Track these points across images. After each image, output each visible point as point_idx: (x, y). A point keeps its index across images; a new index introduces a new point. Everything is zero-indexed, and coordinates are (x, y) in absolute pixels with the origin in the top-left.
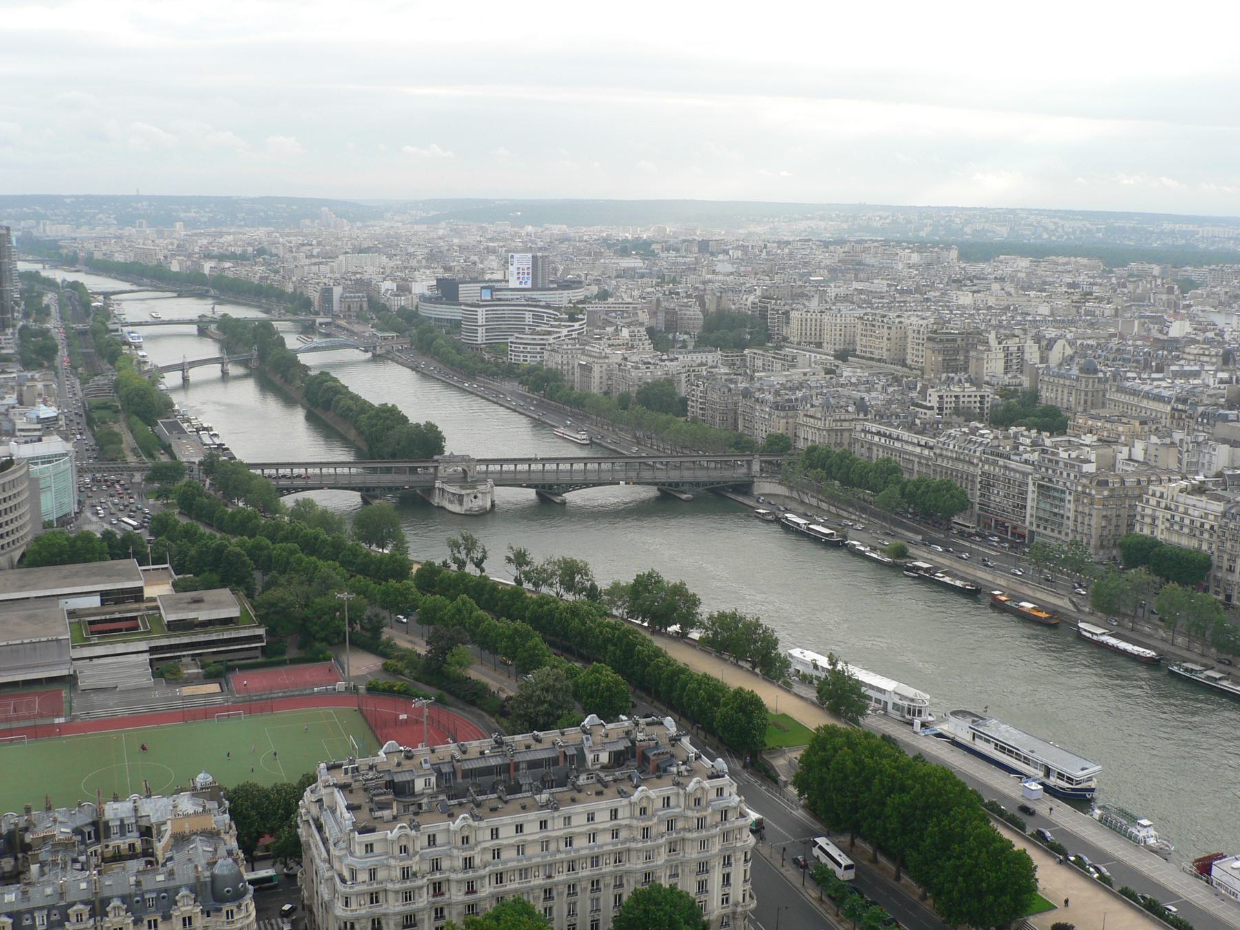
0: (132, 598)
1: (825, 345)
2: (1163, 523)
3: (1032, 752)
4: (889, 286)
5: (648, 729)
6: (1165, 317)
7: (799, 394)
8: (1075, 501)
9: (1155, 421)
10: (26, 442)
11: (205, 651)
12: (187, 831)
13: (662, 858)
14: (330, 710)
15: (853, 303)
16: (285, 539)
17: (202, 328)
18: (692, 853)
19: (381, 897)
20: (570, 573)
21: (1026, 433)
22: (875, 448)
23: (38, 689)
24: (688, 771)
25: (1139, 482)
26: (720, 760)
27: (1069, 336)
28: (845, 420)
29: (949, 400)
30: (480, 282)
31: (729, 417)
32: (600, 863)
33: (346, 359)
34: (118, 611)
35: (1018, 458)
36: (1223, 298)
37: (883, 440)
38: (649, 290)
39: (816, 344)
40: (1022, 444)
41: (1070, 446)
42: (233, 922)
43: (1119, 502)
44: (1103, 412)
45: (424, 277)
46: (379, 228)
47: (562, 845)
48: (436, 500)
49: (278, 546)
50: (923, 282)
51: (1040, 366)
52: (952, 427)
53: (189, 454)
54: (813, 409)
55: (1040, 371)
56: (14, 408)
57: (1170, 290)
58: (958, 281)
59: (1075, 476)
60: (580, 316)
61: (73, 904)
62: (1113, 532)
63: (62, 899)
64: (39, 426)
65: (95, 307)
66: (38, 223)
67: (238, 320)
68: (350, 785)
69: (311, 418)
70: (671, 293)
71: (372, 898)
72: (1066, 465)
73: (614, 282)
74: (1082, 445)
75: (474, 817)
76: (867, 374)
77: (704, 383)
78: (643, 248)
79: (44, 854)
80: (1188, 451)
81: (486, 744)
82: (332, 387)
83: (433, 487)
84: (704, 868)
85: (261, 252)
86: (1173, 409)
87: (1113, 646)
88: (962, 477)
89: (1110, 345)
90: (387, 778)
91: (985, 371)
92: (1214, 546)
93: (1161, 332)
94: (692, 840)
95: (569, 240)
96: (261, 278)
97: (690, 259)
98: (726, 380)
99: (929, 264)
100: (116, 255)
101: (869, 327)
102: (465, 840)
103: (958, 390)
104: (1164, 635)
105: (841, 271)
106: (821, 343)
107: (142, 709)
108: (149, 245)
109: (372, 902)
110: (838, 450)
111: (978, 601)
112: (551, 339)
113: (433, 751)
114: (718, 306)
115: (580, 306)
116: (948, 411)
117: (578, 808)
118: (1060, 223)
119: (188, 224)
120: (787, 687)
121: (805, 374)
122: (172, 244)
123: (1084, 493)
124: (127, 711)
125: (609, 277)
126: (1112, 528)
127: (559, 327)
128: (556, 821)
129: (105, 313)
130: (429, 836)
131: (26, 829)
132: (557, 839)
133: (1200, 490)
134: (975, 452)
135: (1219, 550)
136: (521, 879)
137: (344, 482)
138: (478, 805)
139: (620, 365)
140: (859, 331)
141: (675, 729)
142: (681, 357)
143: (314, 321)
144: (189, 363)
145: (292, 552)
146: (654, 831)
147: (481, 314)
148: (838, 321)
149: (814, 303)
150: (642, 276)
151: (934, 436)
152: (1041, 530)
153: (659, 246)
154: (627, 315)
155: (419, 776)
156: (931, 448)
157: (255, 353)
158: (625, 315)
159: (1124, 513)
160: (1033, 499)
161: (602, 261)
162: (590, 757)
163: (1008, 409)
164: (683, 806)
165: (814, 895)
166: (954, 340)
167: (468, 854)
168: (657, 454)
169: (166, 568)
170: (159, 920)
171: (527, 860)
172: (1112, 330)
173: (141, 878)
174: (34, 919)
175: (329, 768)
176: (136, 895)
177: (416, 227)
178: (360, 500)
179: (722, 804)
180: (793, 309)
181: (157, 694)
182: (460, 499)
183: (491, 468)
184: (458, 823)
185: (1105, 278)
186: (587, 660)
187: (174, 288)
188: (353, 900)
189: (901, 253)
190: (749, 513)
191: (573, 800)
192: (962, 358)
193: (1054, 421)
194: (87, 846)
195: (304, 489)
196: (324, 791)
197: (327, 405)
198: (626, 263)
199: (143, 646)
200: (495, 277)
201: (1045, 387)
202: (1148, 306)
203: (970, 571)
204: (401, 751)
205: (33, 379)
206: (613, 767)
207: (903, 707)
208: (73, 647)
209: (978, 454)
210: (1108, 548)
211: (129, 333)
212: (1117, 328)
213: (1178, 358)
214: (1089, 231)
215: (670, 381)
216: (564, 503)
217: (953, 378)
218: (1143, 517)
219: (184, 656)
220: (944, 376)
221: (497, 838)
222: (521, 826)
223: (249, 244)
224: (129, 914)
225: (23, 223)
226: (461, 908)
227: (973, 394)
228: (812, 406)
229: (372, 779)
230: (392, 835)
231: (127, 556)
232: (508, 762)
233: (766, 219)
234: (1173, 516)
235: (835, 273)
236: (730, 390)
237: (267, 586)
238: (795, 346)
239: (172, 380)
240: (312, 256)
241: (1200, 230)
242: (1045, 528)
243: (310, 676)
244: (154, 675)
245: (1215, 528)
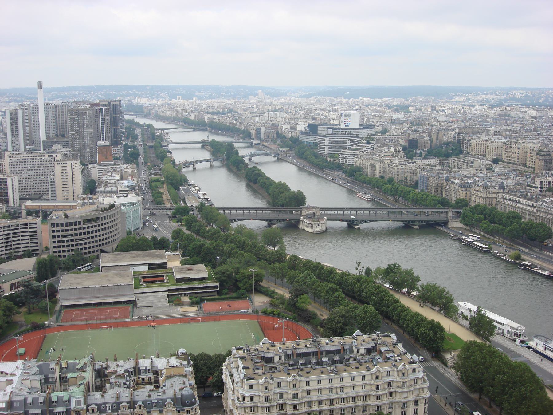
1: (487, 156)
5: (383, 338)
7: (472, 180)
10: (121, 197)
11: (192, 292)
12: (172, 374)
15: (502, 136)
16: (231, 242)
17: (204, 145)
18: (399, 399)
19: (256, 409)
22: (508, 207)
26: (415, 355)
28: (494, 193)
30: (327, 125)
31: (439, 191)
32: (323, 404)
37: (512, 203)
38: (405, 129)
39: (483, 155)
45: (302, 123)
47: (339, 390)
49: (227, 245)
53: (192, 203)
54: (479, 187)
56: (118, 181)
60: (372, 142)
63: (118, 400)
64: (128, 189)
66: (135, 98)
67: (218, 142)
68: (245, 358)
69: (248, 186)
71: (251, 409)
73: (390, 125)
76: (506, 171)
79: (112, 379)
81: (308, 342)
85: (231, 111)
88: (549, 222)
90: (262, 355)
95: (370, 105)
96: (230, 123)
99: (542, 117)
100: (167, 112)
101: (509, 148)
103: (550, 179)
109: (251, 411)
110: (490, 207)
115: (373, 137)
119: (200, 98)
120: (456, 321)
122: (192, 107)
125: (388, 123)
127: (362, 146)
128: (336, 379)
129: (161, 138)
130: (278, 383)
132: (337, 388)
136: (319, 405)
139: (389, 165)
140: (504, 150)
142: (418, 161)
144: (196, 161)
145: (233, 249)
146: (382, 387)
147: (327, 140)
148: (494, 145)
149: (483, 137)
151: (537, 202)
155: (277, 355)
156: (535, 207)
157: (225, 157)
158: (393, 141)
162: (355, 350)
167: (295, 392)
174: (106, 407)
175: (236, 349)
176: (148, 401)
179: (415, 376)
180: (472, 139)
186: (363, 302)
190: (446, 235)
191: (345, 370)
197: (255, 182)
198: (396, 116)
199: (165, 289)
215: (414, 172)
217: (548, 173)
220: (544, 172)
221: (320, 383)
223: (226, 107)
224: (145, 409)
229: (255, 355)
230: (261, 381)
233: (465, 94)
235: (496, 121)
236: (439, 178)
240: (253, 113)
243: (239, 305)
244: (169, 302)
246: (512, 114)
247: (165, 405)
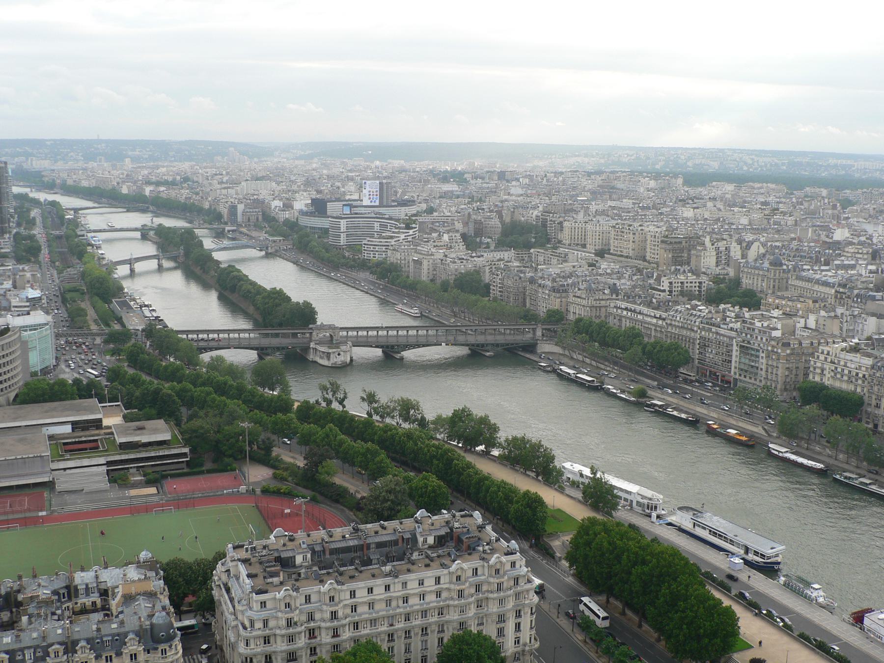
0: (94, 426)
1: (588, 246)
2: (829, 373)
3: (736, 536)
5: (462, 519)
6: (831, 226)
7: (570, 281)
8: (766, 357)
9: (824, 300)
10: (19, 315)
11: (146, 464)
12: (133, 593)
14: (235, 506)
15: (608, 216)
16: (204, 384)
17: (144, 234)
18: (494, 608)
19: (272, 640)
20: (407, 408)
21: (731, 309)
22: (624, 320)
23: (27, 491)
24: (490, 550)
25: (812, 343)
26: (513, 541)
27: (762, 239)
28: (602, 300)
29: (676, 285)
30: (342, 201)
31: (520, 297)
33: (246, 256)
34: (84, 436)
35: (725, 327)
36: (872, 212)
37: (629, 314)
38: (463, 206)
39: (582, 245)
40: (729, 317)
41: (763, 318)
42: (166, 657)
43: (798, 358)
44: (786, 294)
45: (302, 198)
46: (270, 162)
47: (401, 602)
48: (311, 357)
49: (198, 389)
50: (658, 201)
51: (742, 261)
52: (679, 304)
53: (135, 323)
54: (580, 292)
55: (742, 265)
56: (10, 291)
57: (834, 207)
58: (683, 200)
59: (767, 340)
60: (414, 226)
61: (52, 644)
62: (793, 379)
63: (44, 641)
64: (28, 304)
65: (68, 219)
66: (27, 159)
67: (169, 228)
68: (249, 560)
69: (222, 298)
70: (478, 209)
71: (265, 641)
72: (760, 331)
73: (438, 201)
74: (771, 317)
75: (338, 583)
76: (618, 267)
77: (502, 273)
78: (458, 177)
80: (847, 321)
81: (347, 530)
82: (237, 276)
83: (309, 348)
84: (502, 619)
85: (186, 179)
86: (836, 291)
87: (793, 461)
88: (686, 340)
90: (276, 555)
91: (702, 265)
93: (827, 236)
94: (494, 599)
95: (406, 171)
96: (186, 198)
97: (492, 185)
98: (517, 271)
99: (663, 188)
100: (83, 182)
101: (619, 233)
102: (332, 599)
103: (683, 278)
104: (830, 453)
105: (599, 193)
106: (585, 245)
109: (265, 643)
110: (597, 321)
111: (697, 429)
112: (393, 242)
113: (309, 536)
114: (512, 218)
115: (414, 218)
116: (676, 293)
117: (412, 576)
118: (756, 159)
119: (134, 160)
120: (561, 490)
121: (574, 267)
122: (123, 174)
123: (773, 351)
124: (90, 507)
125: (434, 197)
126: (793, 376)
127: (398, 233)
128: (396, 585)
129: (75, 223)
130: (306, 596)
131: (19, 591)
132: (397, 598)
133: (855, 349)
134: (695, 322)
135: (869, 392)
136: (371, 627)
137: (246, 343)
138: (341, 574)
139: (442, 260)
140: (612, 236)
142: (485, 254)
143: (224, 229)
144: (135, 259)
145: (208, 394)
146: (466, 593)
147: (343, 224)
148: (598, 229)
149: (580, 216)
150: (458, 197)
151: (666, 311)
152: (742, 378)
153: (470, 176)
154: (447, 224)
155: (299, 553)
156: (664, 319)
157: (182, 252)
158: (446, 224)
160: (737, 356)
161: (429, 186)
162: (420, 540)
163: (719, 292)
164: (487, 575)
165: (580, 638)
166: (680, 243)
167: (333, 609)
168: (469, 324)
169: (119, 405)
170: (114, 656)
171: (375, 613)
172: (793, 235)
173: (101, 626)
175: (235, 548)
176: (97, 638)
178: (257, 356)
179: (515, 573)
180: (565, 221)
181: (112, 495)
182: (328, 355)
183: (350, 333)
184: (326, 587)
185: (788, 198)
187: (124, 206)
188: (252, 642)
189: (642, 180)
190: (534, 366)
191: (409, 571)
192: (686, 255)
195: (217, 349)
197: (233, 289)
198: (446, 187)
199: (102, 460)
200: (353, 197)
201: (745, 276)
202: (818, 218)
203: (691, 407)
204: (286, 535)
205: (23, 270)
206: (437, 547)
207: (644, 504)
208: (52, 461)
209: (697, 324)
210: (790, 391)
211: (92, 237)
212: (796, 234)
213: (840, 255)
214: (776, 164)
215: (478, 272)
216: (402, 359)
217: (679, 270)
218: (815, 368)
219: (131, 468)
220: (673, 268)
221: (354, 597)
222: (372, 589)
223: (178, 174)
224: (92, 651)
225: (16, 159)
226: (329, 647)
227: (694, 281)
228: (579, 289)
229: (265, 556)
230: (280, 595)
232: (362, 543)
233: (546, 156)
234: (836, 368)
235: (595, 194)
236: (520, 278)
237: (190, 418)
238: (567, 246)
239: (122, 271)
240: (222, 183)
241: (856, 164)
242: (745, 377)
243: (221, 482)
244: (110, 481)
245: (866, 376)
246: (619, 185)
247: (125, 644)
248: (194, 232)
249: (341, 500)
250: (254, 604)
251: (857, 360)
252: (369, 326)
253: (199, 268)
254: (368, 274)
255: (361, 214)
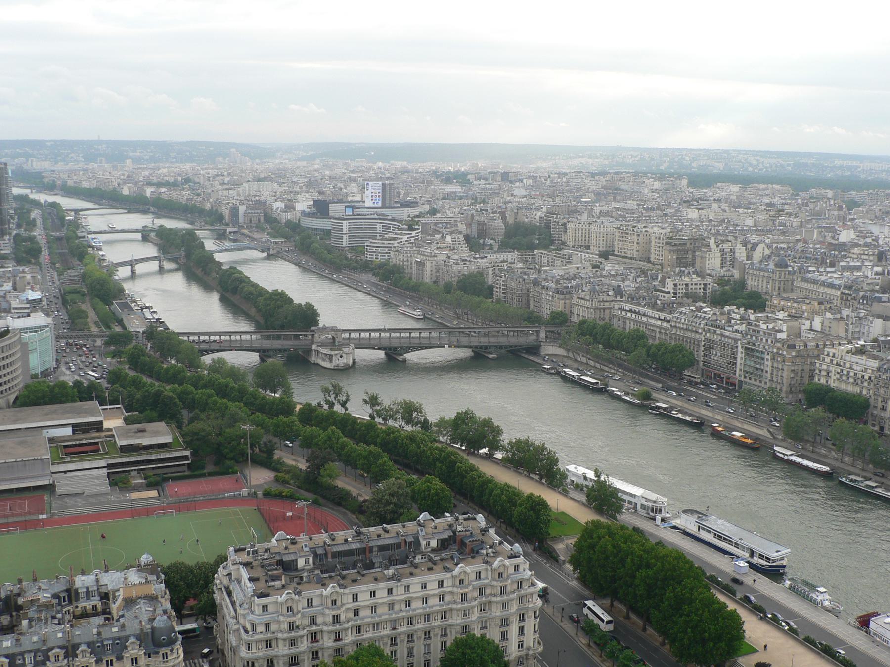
0: (94, 429)
1: (592, 247)
2: (835, 375)
3: (741, 539)
4: (638, 205)
5: (465, 523)
8: (771, 359)
9: (829, 302)
10: (19, 317)
11: (147, 467)
12: (134, 596)
13: (475, 615)
14: (237, 509)
15: (612, 217)
16: (205, 387)
17: (145, 235)
18: (497, 612)
19: (274, 644)
20: (409, 411)
21: (736, 311)
22: (628, 322)
23: (28, 494)
24: (494, 553)
25: (817, 345)
26: (517, 545)
27: (767, 241)
28: (607, 302)
29: (681, 287)
30: (344, 202)
31: (523, 299)
33: (248, 258)
34: (85, 439)
35: (730, 329)
36: (878, 214)
37: (634, 316)
38: (466, 208)
39: (585, 246)
40: (733, 319)
41: (768, 320)
42: (167, 661)
43: (803, 360)
44: (792, 296)
45: (304, 199)
46: (272, 163)
47: (403, 606)
48: (313, 359)
51: (747, 262)
52: (683, 306)
53: (136, 325)
54: (584, 294)
55: (747, 266)
56: (10, 292)
57: (840, 208)
58: (688, 202)
59: (772, 342)
60: (416, 227)
61: (53, 648)
62: (799, 382)
63: (44, 644)
64: (28, 306)
65: (68, 220)
66: (27, 160)
67: (171, 229)
68: (251, 563)
69: (223, 300)
70: (481, 210)
71: (267, 644)
72: (765, 333)
73: (441, 202)
74: (777, 319)
75: (341, 586)
76: (622, 268)
77: (505, 275)
78: (461, 178)
80: (852, 323)
81: (349, 534)
82: (238, 278)
83: (311, 350)
84: (505, 622)
85: (187, 180)
86: (842, 293)
87: (799, 463)
88: (690, 342)
89: (797, 248)
90: (278, 558)
91: (707, 266)
92: (871, 392)
93: (833, 238)
94: (497, 603)
95: (408, 172)
96: (187, 199)
97: (495, 186)
98: (521, 273)
99: (667, 190)
100: (84, 183)
101: (624, 235)
102: (334, 602)
103: (688, 280)
104: (836, 455)
105: (603, 194)
106: (589, 246)
107: (102, 508)
108: (107, 176)
109: (267, 647)
110: (601, 323)
111: (702, 431)
112: (395, 243)
113: (311, 539)
114: (516, 219)
115: (416, 219)
116: (681, 295)
117: (415, 579)
118: (761, 160)
119: (135, 160)
120: (565, 493)
121: (578, 268)
122: (123, 175)
123: (778, 353)
124: (91, 510)
125: (437, 199)
126: (798, 378)
127: (401, 234)
128: (399, 589)
129: (76, 225)
130: (308, 600)
131: (19, 595)
132: (400, 602)
133: (861, 351)
134: (700, 324)
136: (374, 630)
137: (247, 346)
138: (343, 577)
139: (445, 262)
140: (617, 238)
141: (484, 523)
142: (489, 256)
143: (226, 230)
144: (136, 260)
145: (210, 396)
146: (469, 596)
147: (345, 225)
148: (602, 230)
149: (584, 218)
150: (461, 198)
151: (671, 313)
152: (747, 380)
153: (473, 177)
155: (301, 557)
156: (669, 321)
157: (183, 253)
158: (449, 226)
159: (807, 368)
160: (742, 358)
162: (423, 543)
163: (724, 293)
164: (490, 578)
165: (584, 642)
166: (685, 244)
167: (336, 612)
168: (472, 325)
169: (119, 408)
170: (114, 660)
171: (378, 617)
172: (798, 237)
173: (101, 630)
175: (236, 551)
176: (98, 642)
177: (299, 163)
178: (258, 358)
179: (518, 576)
180: (569, 222)
181: (113, 498)
182: (330, 358)
183: (353, 335)
184: (329, 590)
185: (793, 199)
188: (254, 646)
189: (647, 181)
190: (537, 368)
191: (412, 574)
192: (691, 257)
193: (756, 302)
194: (63, 607)
195: (218, 351)
196: (232, 567)
197: (235, 291)
198: (449, 188)
199: (103, 463)
200: (355, 199)
201: (750, 277)
202: (824, 219)
203: (696, 409)
204: (288, 539)
205: (23, 272)
206: (440, 550)
207: (648, 507)
208: (53, 464)
209: (702, 326)
210: (795, 393)
211: (93, 239)
212: (801, 235)
214: (782, 165)
215: (481, 273)
216: (405, 361)
217: (684, 271)
218: (820, 371)
219: (132, 470)
220: (678, 270)
221: (357, 601)
222: (374, 592)
223: (179, 175)
224: (93, 655)
225: (16, 160)
226: (331, 651)
227: (699, 283)
228: (583, 291)
229: (267, 559)
230: (281, 599)
231: (91, 399)
232: (364, 546)
233: (549, 157)
234: (842, 370)
235: (599, 196)
236: (524, 280)
237: (192, 421)
238: (571, 248)
239: (123, 272)
240: (224, 184)
241: (861, 165)
242: (750, 379)
243: (223, 485)
244: (111, 484)
245: (872, 379)
246: (624, 186)
248: (195, 233)
249: (343, 503)
250: (256, 608)
251: (863, 362)
252: (371, 328)
253: (201, 269)
254: (371, 275)
255: (364, 215)
